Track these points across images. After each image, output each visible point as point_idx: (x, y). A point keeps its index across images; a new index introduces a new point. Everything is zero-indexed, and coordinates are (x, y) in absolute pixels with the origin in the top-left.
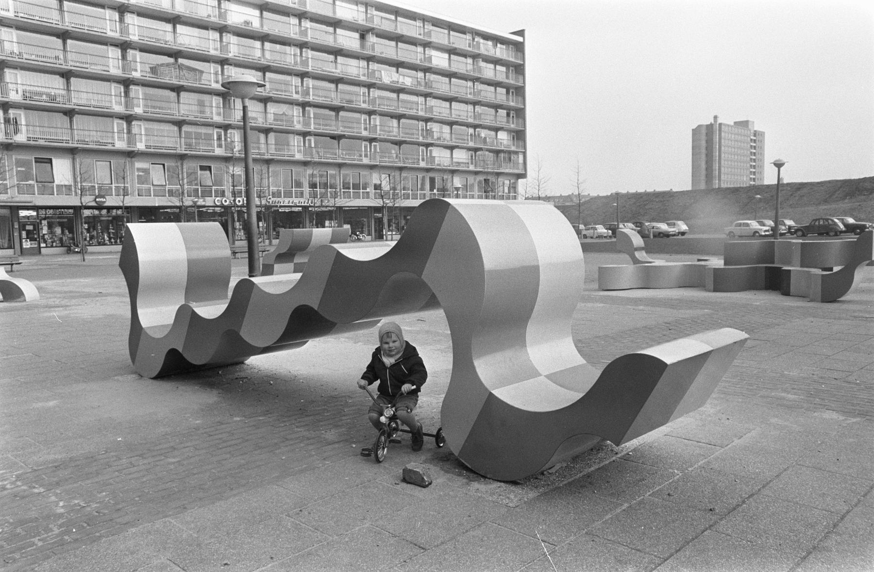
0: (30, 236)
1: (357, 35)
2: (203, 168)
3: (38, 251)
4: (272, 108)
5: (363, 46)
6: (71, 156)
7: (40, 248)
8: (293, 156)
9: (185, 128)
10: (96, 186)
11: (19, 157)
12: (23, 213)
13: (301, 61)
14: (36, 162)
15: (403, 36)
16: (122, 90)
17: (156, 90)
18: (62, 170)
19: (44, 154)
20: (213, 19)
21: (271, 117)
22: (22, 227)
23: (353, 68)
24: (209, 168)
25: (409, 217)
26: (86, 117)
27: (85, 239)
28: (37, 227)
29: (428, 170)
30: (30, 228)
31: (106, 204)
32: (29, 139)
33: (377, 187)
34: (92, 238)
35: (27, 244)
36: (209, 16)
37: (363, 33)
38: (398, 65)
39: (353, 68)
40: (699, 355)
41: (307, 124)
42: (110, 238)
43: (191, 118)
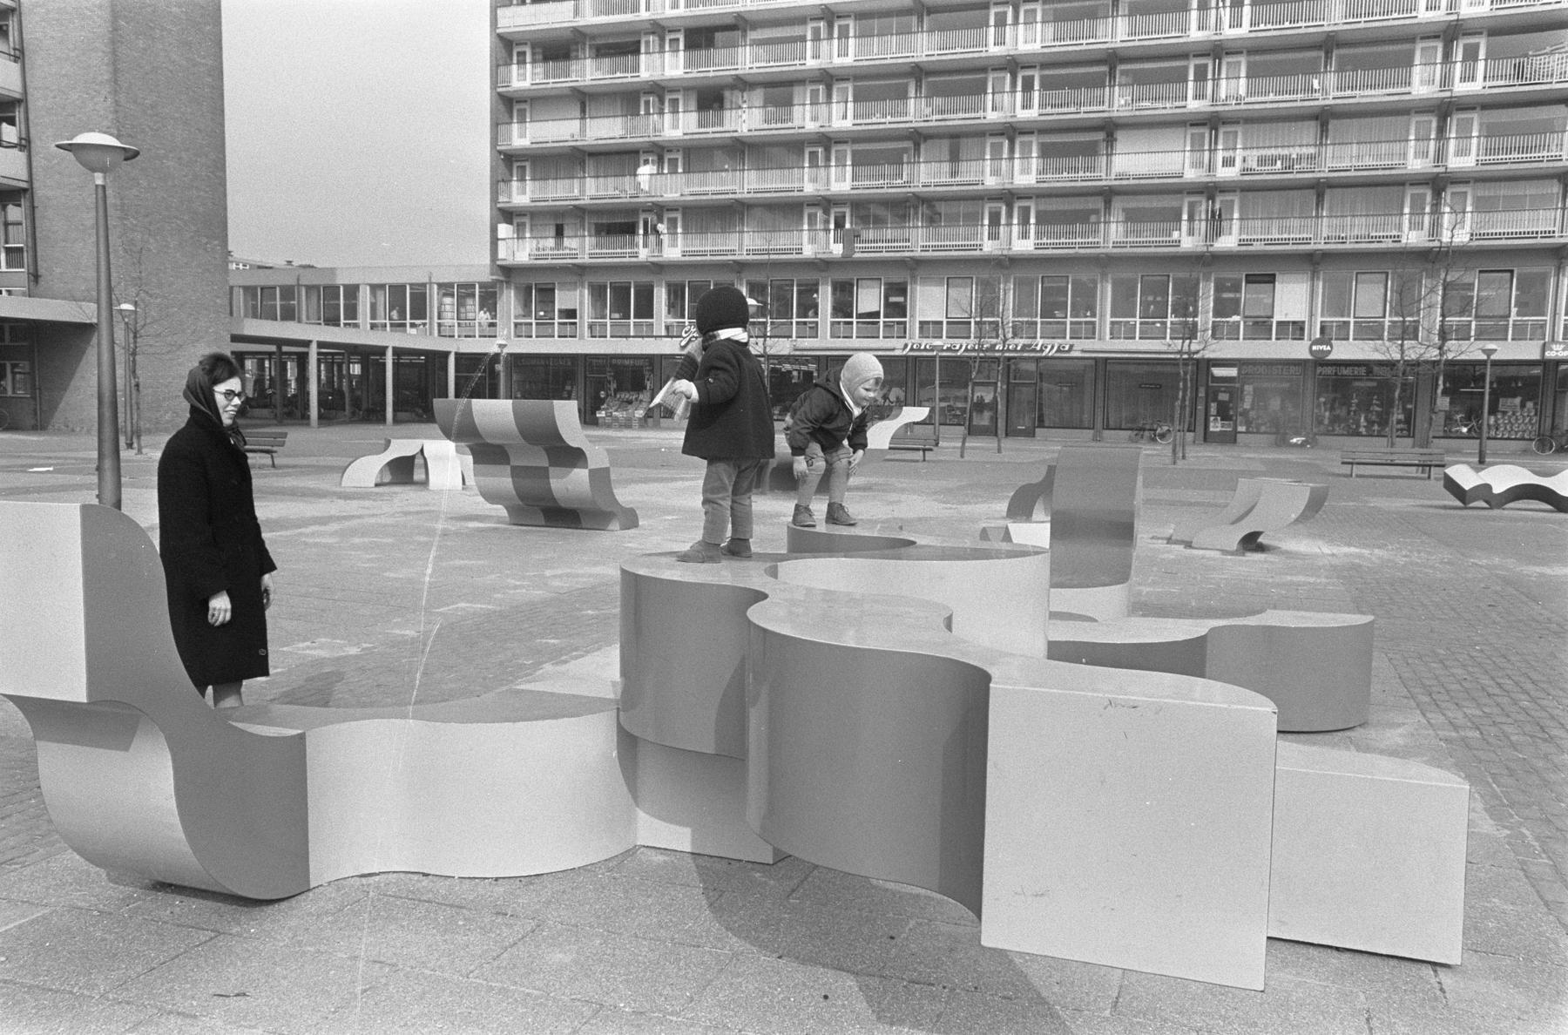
0: (1224, 414)
3: (1229, 439)
6: (1556, 262)
7: (1236, 432)
10: (1352, 320)
11: (1528, 270)
12: (1218, 372)
14: (1248, 282)
16: (1434, 125)
17: (1511, 111)
18: (929, 302)
19: (899, 279)
22: (1212, 395)
25: (356, 369)
26: (1349, 190)
27: (1320, 423)
28: (1237, 395)
30: (1223, 397)
31: (1331, 357)
32: (1241, 243)
35: (1216, 426)
40: (305, 772)
42: (1370, 423)
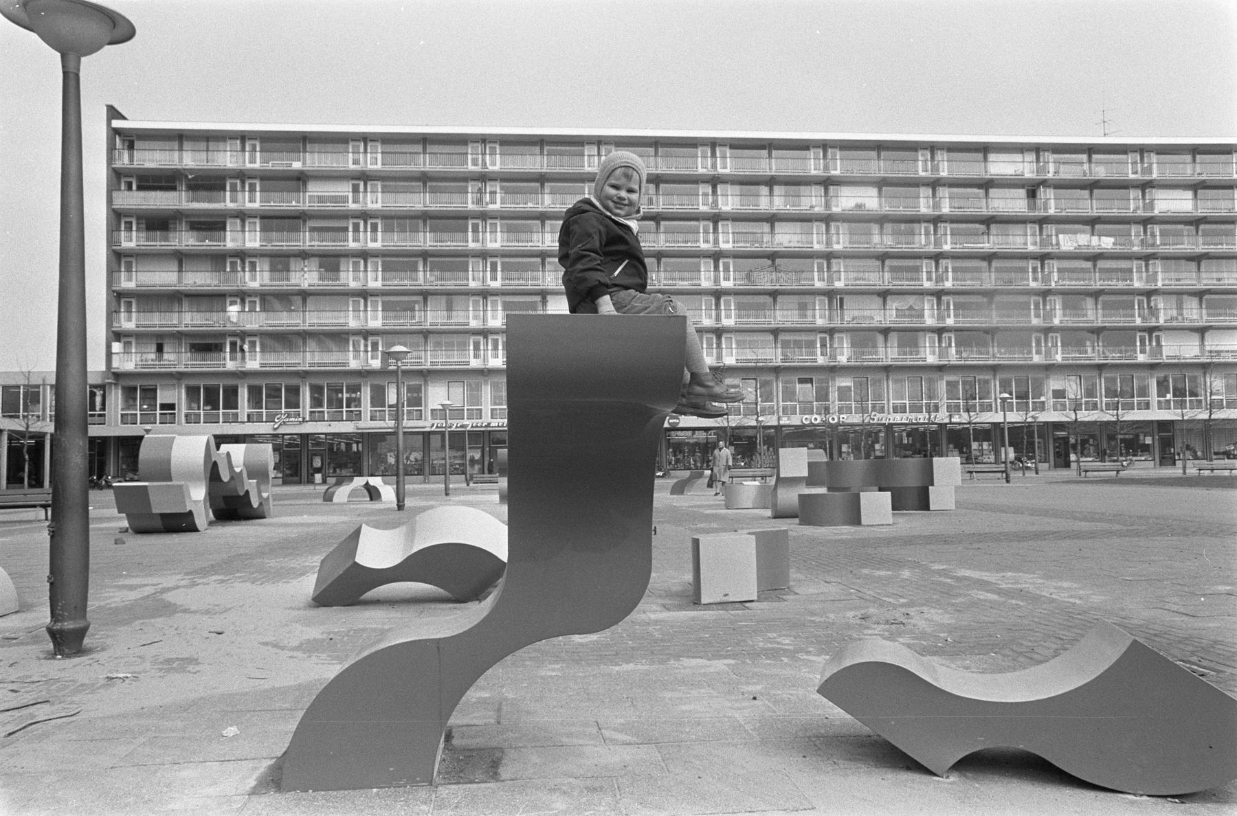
1: (1022, 193)
2: (802, 381)
4: (894, 304)
5: (1032, 207)
8: (468, 363)
9: (781, 337)
13: (1145, 204)
15: (1098, 181)
20: (817, 210)
21: (847, 318)
23: (1025, 240)
24: (810, 381)
29: (1152, 367)
32: (262, 365)
33: (1059, 394)
34: (677, 461)
36: (812, 207)
37: (1032, 189)
38: (1092, 223)
39: (1025, 240)
41: (940, 318)
43: (788, 325)
